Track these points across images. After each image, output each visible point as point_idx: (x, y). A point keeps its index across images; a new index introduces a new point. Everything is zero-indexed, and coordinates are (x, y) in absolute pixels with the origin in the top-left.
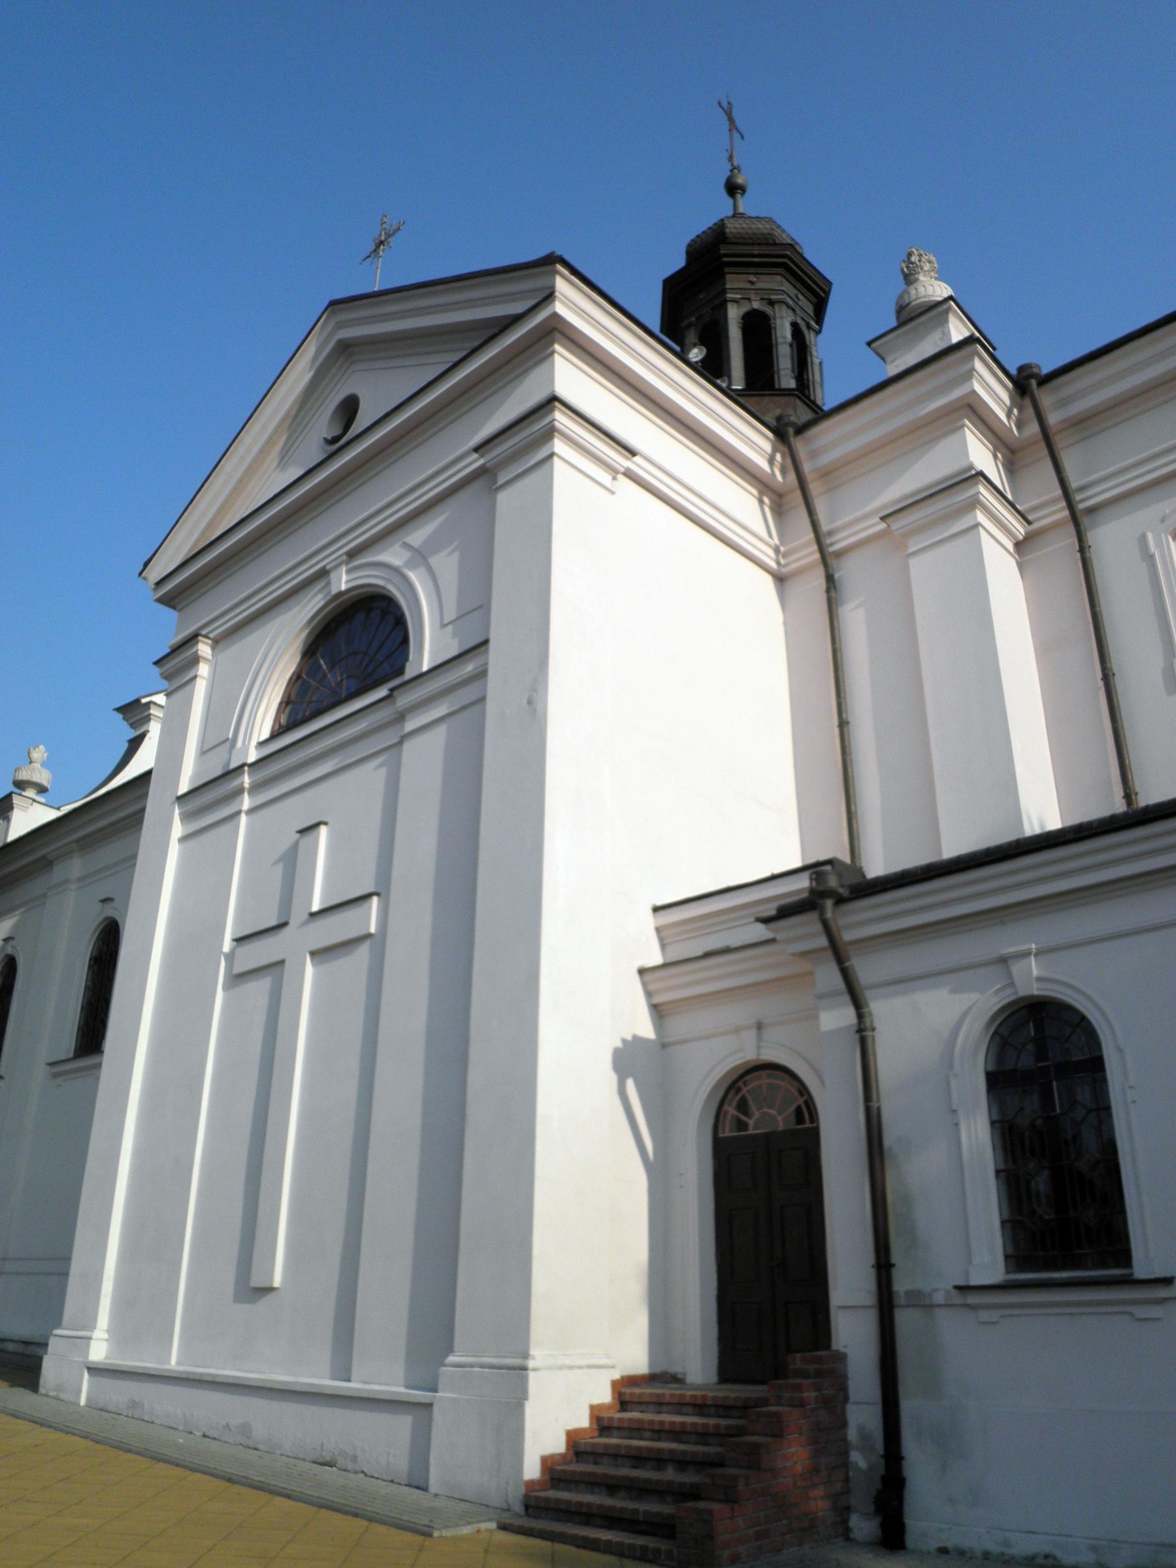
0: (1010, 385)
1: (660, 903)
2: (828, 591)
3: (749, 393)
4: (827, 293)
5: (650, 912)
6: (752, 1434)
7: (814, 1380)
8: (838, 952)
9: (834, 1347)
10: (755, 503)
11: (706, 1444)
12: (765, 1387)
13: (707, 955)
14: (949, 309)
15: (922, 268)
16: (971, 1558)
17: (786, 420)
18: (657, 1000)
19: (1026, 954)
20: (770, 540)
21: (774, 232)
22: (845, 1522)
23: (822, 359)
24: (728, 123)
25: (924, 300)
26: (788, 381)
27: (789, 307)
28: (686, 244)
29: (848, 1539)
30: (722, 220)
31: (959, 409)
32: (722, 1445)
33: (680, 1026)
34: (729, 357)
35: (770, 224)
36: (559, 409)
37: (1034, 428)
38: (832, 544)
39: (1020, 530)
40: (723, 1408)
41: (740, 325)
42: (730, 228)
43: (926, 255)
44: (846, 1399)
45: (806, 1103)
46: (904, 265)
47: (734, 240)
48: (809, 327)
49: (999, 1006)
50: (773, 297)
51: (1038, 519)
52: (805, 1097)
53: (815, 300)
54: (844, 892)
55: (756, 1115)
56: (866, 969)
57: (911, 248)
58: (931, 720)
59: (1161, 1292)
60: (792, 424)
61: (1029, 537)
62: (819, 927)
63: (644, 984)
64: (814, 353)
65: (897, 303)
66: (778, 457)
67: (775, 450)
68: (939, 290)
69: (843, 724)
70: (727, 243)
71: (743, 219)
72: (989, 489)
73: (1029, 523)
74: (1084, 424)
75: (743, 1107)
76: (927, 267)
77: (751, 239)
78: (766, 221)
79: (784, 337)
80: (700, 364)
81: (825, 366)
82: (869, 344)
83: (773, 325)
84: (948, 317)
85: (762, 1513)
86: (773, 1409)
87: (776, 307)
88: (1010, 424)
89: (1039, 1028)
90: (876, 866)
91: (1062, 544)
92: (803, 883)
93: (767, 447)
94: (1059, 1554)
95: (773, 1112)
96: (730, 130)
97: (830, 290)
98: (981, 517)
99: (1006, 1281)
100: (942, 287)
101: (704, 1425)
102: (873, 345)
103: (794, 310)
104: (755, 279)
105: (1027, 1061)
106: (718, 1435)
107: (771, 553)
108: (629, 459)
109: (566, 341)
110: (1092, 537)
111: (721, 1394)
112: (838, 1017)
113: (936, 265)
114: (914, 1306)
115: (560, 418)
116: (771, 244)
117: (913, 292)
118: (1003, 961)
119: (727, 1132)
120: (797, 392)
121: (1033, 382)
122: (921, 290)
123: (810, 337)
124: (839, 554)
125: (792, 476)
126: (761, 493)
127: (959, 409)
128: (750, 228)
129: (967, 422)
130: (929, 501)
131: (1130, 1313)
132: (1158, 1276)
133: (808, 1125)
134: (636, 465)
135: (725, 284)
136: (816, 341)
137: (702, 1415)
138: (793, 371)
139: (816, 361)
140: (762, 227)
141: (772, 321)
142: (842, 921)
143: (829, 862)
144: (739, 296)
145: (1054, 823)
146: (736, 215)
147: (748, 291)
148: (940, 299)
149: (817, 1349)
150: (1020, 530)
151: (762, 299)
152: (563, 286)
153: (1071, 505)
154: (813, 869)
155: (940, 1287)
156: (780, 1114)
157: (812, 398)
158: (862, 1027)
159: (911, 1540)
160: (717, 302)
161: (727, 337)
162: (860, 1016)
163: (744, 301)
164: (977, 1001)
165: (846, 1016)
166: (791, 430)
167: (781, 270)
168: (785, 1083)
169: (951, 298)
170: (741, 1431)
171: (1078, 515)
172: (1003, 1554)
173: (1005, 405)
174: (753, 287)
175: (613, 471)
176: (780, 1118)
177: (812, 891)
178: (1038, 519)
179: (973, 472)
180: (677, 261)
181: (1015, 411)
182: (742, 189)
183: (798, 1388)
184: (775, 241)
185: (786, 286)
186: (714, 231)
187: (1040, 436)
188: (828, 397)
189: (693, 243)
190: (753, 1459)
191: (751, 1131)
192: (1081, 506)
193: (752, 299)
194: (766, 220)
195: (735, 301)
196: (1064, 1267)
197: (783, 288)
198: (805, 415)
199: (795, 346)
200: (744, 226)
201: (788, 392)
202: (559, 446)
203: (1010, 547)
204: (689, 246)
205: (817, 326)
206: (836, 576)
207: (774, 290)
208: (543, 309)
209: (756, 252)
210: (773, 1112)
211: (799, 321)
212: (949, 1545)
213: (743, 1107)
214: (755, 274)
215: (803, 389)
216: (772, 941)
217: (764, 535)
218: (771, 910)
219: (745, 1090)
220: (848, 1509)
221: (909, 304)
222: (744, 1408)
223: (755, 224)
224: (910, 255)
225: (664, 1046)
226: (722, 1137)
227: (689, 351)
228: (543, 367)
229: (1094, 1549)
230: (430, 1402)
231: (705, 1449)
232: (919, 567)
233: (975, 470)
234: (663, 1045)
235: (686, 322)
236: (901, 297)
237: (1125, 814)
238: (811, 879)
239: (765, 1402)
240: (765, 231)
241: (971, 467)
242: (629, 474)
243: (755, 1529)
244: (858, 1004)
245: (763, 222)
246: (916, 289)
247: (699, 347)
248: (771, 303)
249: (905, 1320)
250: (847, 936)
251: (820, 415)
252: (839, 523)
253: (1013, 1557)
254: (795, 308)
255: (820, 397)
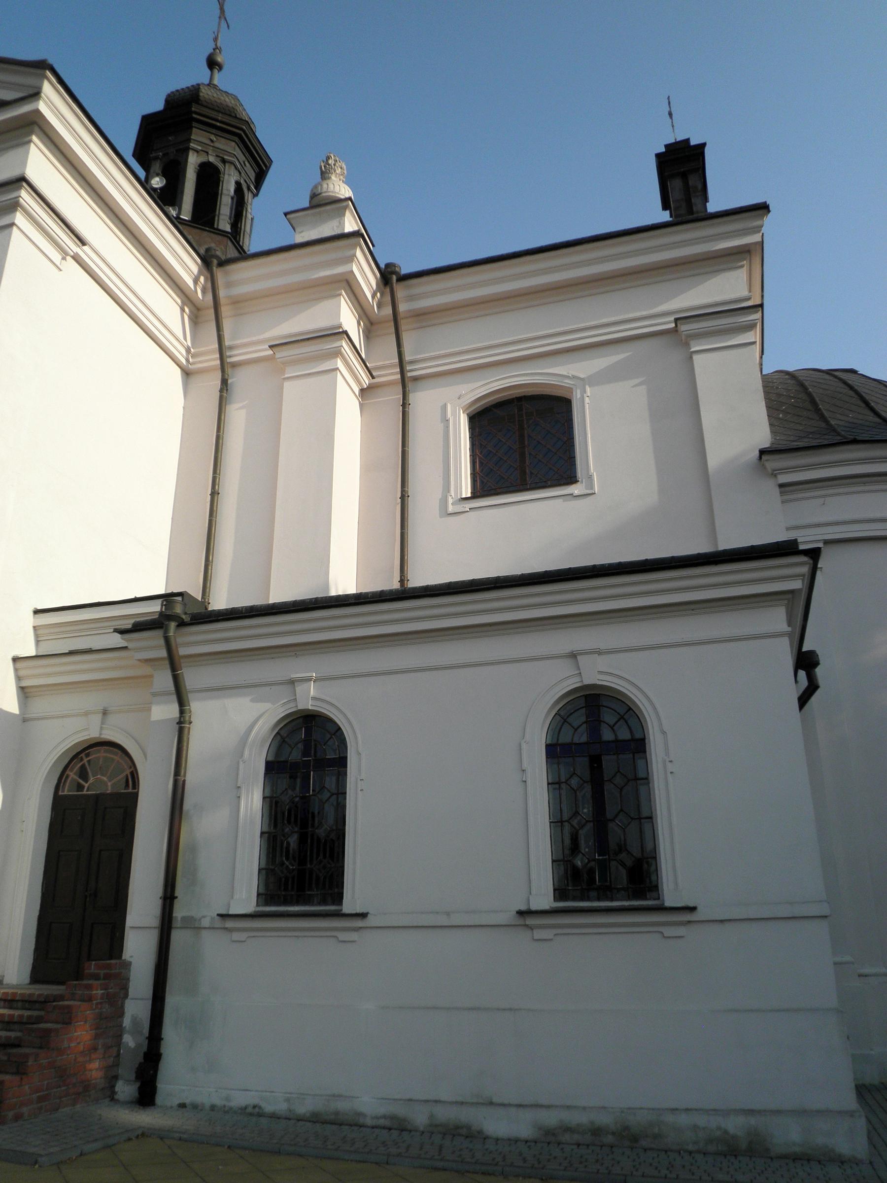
0: (378, 275)
1: (39, 608)
2: (221, 391)
3: (192, 224)
4: (268, 168)
5: (32, 613)
6: (46, 1022)
7: (103, 981)
8: (173, 663)
9: (123, 958)
10: (178, 310)
11: (10, 1030)
12: (63, 987)
13: (71, 653)
14: (347, 207)
15: (335, 171)
16: (201, 1110)
17: (213, 253)
18: (24, 683)
19: (308, 680)
20: (184, 341)
21: (236, 108)
22: (113, 1087)
23: (254, 217)
24: (219, 11)
25: (331, 194)
26: (224, 224)
27: (236, 168)
28: (166, 94)
29: (112, 1099)
30: (198, 85)
31: (340, 281)
32: (20, 1031)
33: (40, 706)
34: (182, 192)
35: (234, 101)
36: (25, 188)
37: (388, 311)
38: (230, 357)
39: (366, 380)
40: (28, 1002)
41: (197, 170)
42: (203, 93)
43: (340, 162)
44: (126, 996)
45: (132, 774)
46: (323, 164)
47: (205, 104)
48: (249, 188)
49: (283, 715)
50: (226, 157)
51: (379, 376)
52: (132, 769)
53: (257, 170)
54: (186, 618)
55: (92, 779)
56: (192, 678)
57: (330, 153)
58: (278, 503)
59: (359, 923)
60: (217, 257)
61: (370, 387)
62: (162, 642)
63: (16, 670)
64: (249, 210)
65: (312, 190)
66: (202, 279)
67: (200, 273)
68: (344, 191)
69: (214, 494)
70: (199, 104)
71: (215, 89)
72: (349, 345)
73: (373, 377)
74: (422, 316)
75: (83, 774)
76: (339, 171)
77: (218, 107)
78: (232, 97)
79: (229, 190)
80: (159, 191)
81: (255, 220)
82: (286, 214)
83: (221, 179)
84: (346, 211)
85: (46, 1082)
86: (66, 1003)
87: (227, 165)
88: (373, 302)
89: (308, 733)
90: (219, 602)
91: (394, 397)
92: (156, 607)
93: (195, 269)
94: (263, 1105)
95: (105, 779)
96: (220, 17)
97: (270, 166)
98: (340, 364)
99: (255, 912)
100: (346, 190)
101: (10, 1015)
102: (288, 216)
103: (240, 173)
104: (215, 139)
105: (296, 755)
106: (21, 1022)
107: (184, 352)
108: (79, 246)
109: (42, 135)
110: (413, 398)
111: (28, 992)
112: (165, 711)
113: (345, 172)
114: (187, 928)
115: (25, 196)
116: (233, 117)
117: (325, 186)
118: (292, 682)
119: (65, 792)
120: (229, 235)
121: (394, 278)
122: (331, 186)
123: (248, 196)
124: (234, 365)
125: (210, 296)
126: (183, 303)
127: (340, 281)
128: (219, 99)
129: (343, 293)
130: (307, 343)
131: (336, 937)
132: (358, 912)
133: (130, 790)
134: (84, 253)
135: (191, 134)
136: (252, 202)
137: (11, 1008)
138: (230, 218)
139: (249, 216)
140: (228, 101)
141: (222, 175)
142: (180, 640)
143: (180, 594)
144: (200, 148)
145: (352, 589)
146: (210, 84)
147: (208, 147)
148: (342, 197)
149: (111, 958)
150: (366, 380)
151: (217, 156)
152: (49, 90)
153: (402, 372)
154: (167, 598)
155: (208, 913)
156: (110, 781)
157: (241, 244)
158: (182, 720)
159: (159, 1100)
160: (181, 147)
161: (184, 176)
162: (182, 712)
163: (203, 152)
164: (268, 710)
165: (171, 710)
166: (215, 262)
167: (236, 139)
168: (117, 757)
169: (350, 199)
170: (39, 1020)
171: (406, 379)
172: (225, 1106)
173: (373, 289)
174: (212, 145)
175: (64, 253)
176: (109, 784)
177: (161, 613)
178: (379, 376)
179: (341, 330)
180: (157, 105)
181: (378, 294)
182: (220, 67)
183: (89, 987)
184: (236, 116)
185: (238, 152)
186: (191, 91)
187: (392, 317)
188: (253, 244)
189: (172, 95)
190: (44, 1040)
191: (85, 792)
192: (409, 374)
193: (210, 153)
194: (233, 97)
195: (197, 151)
196: (298, 903)
197: (235, 153)
198: (232, 253)
199: (235, 200)
200: (215, 95)
201: (223, 233)
202: (19, 218)
203: (357, 391)
204: (169, 96)
205: (255, 190)
206: (229, 381)
207: (226, 151)
208: (30, 103)
209: (220, 118)
210: (105, 779)
211: (242, 182)
212: (187, 1101)
213: (83, 774)
214: (215, 135)
215: (236, 234)
216: (126, 648)
217: (181, 337)
218: (128, 624)
219: (85, 760)
220: (116, 1078)
221: (320, 194)
222: (42, 1003)
223: (223, 97)
224: (328, 158)
225: (25, 720)
226: (61, 795)
227: (153, 177)
228: (20, 151)
229: (288, 1100)
230: (695, 906)
231: (9, 1034)
232: (291, 390)
233: (342, 328)
234: (24, 719)
235: (153, 155)
236: (316, 187)
237: (397, 591)
238: (162, 605)
239: (61, 998)
240: (230, 105)
241: (340, 326)
242: (76, 258)
243: (38, 1094)
244: (182, 702)
245: (230, 98)
246: (328, 184)
247: (160, 176)
248: (224, 161)
249: (178, 937)
250: (182, 651)
251: (244, 256)
252: (238, 342)
253: (231, 1108)
254: (241, 172)
255: (248, 244)
